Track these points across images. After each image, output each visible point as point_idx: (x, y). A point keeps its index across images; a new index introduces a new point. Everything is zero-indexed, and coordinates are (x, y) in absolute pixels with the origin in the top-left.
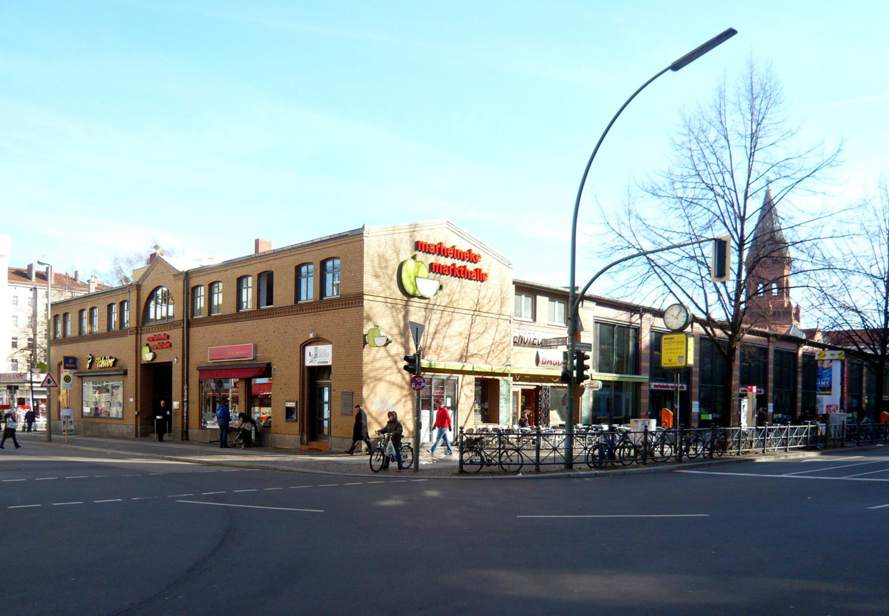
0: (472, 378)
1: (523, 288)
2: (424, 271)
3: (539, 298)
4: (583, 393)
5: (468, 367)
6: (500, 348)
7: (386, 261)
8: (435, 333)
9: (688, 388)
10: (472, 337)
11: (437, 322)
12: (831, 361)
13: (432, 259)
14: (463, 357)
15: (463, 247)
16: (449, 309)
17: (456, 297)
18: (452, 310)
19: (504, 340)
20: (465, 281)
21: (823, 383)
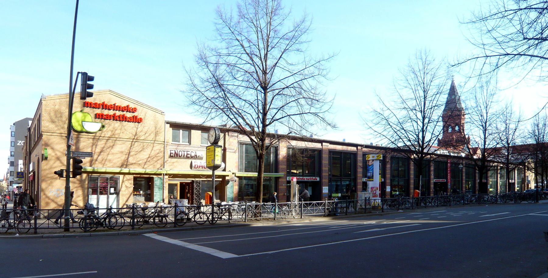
0: (132, 177)
1: (175, 126)
2: (90, 118)
3: (193, 132)
4: (228, 184)
5: (126, 170)
6: (155, 159)
7: (61, 113)
8: (101, 152)
9: (320, 179)
10: (131, 154)
11: (102, 146)
12: (373, 160)
13: (98, 111)
14: (125, 164)
15: (124, 104)
16: (112, 139)
17: (117, 132)
18: (115, 139)
19: (159, 155)
20: (125, 123)
21: (369, 174)
